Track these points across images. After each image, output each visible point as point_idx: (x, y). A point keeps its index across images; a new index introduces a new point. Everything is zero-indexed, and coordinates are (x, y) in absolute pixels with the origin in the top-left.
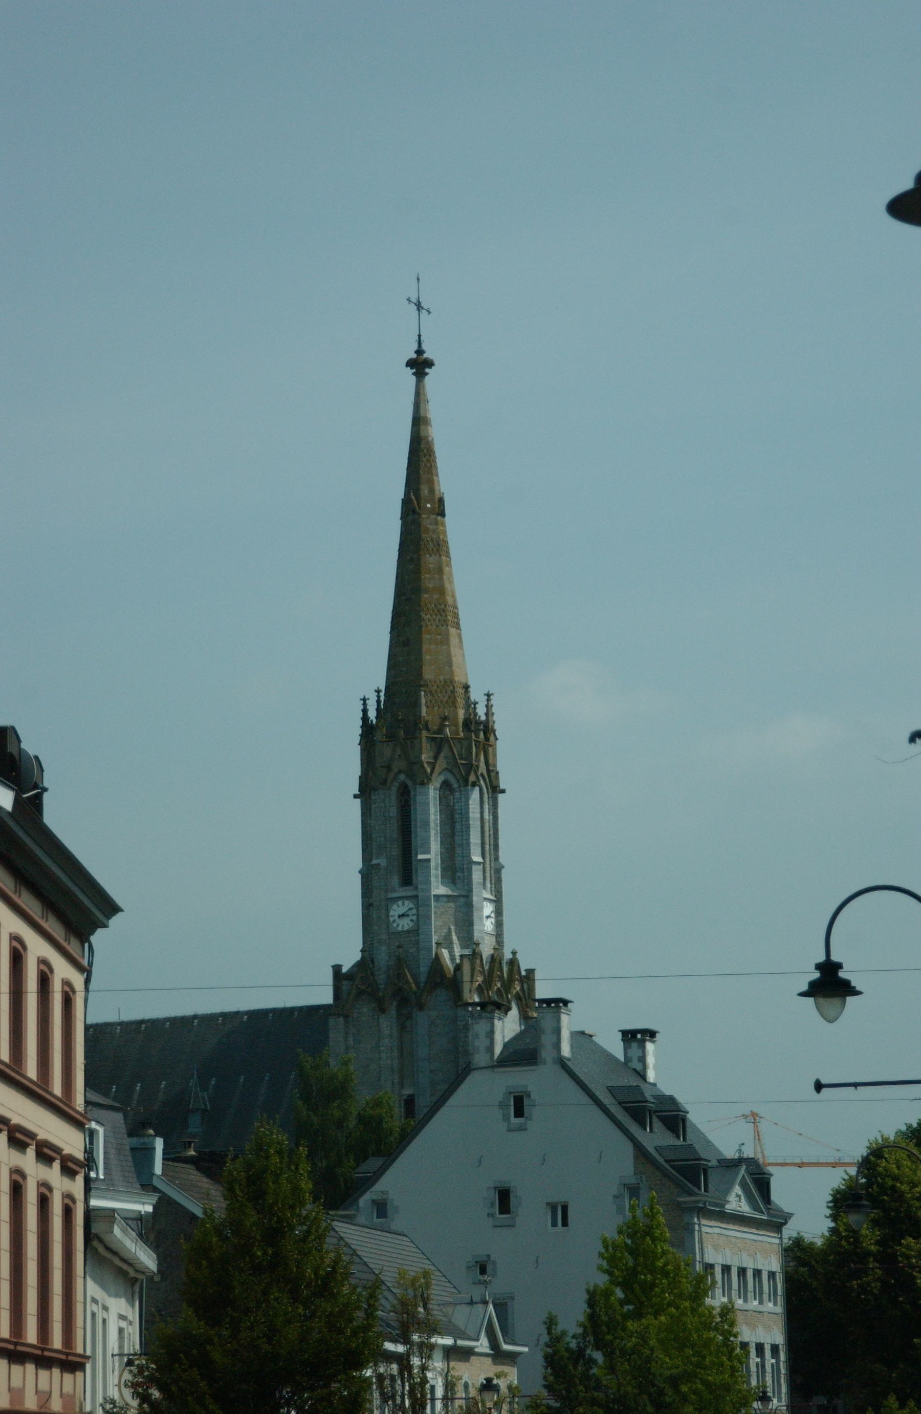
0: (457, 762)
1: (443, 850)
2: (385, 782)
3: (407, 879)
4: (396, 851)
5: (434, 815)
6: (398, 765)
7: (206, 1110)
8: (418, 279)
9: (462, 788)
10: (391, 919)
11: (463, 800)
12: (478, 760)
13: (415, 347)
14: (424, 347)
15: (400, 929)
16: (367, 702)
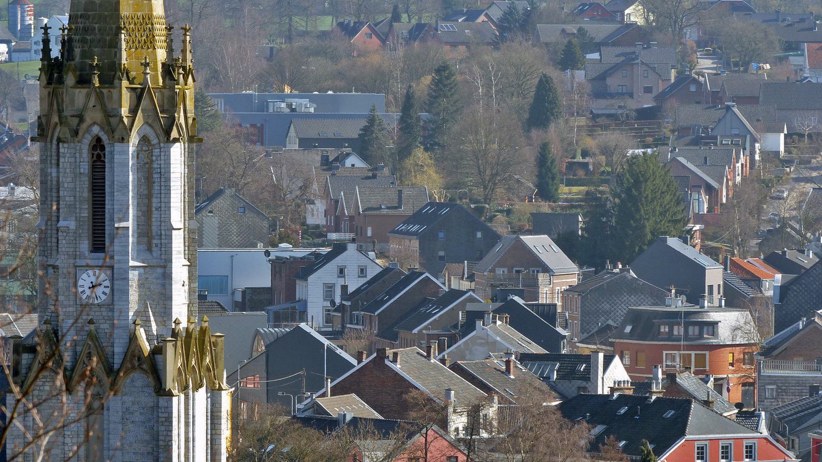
0: (158, 116)
1: (140, 214)
2: (76, 133)
3: (99, 244)
4: (85, 212)
6: (93, 115)
9: (162, 145)
10: (80, 290)
11: (162, 158)
16: (49, 31)
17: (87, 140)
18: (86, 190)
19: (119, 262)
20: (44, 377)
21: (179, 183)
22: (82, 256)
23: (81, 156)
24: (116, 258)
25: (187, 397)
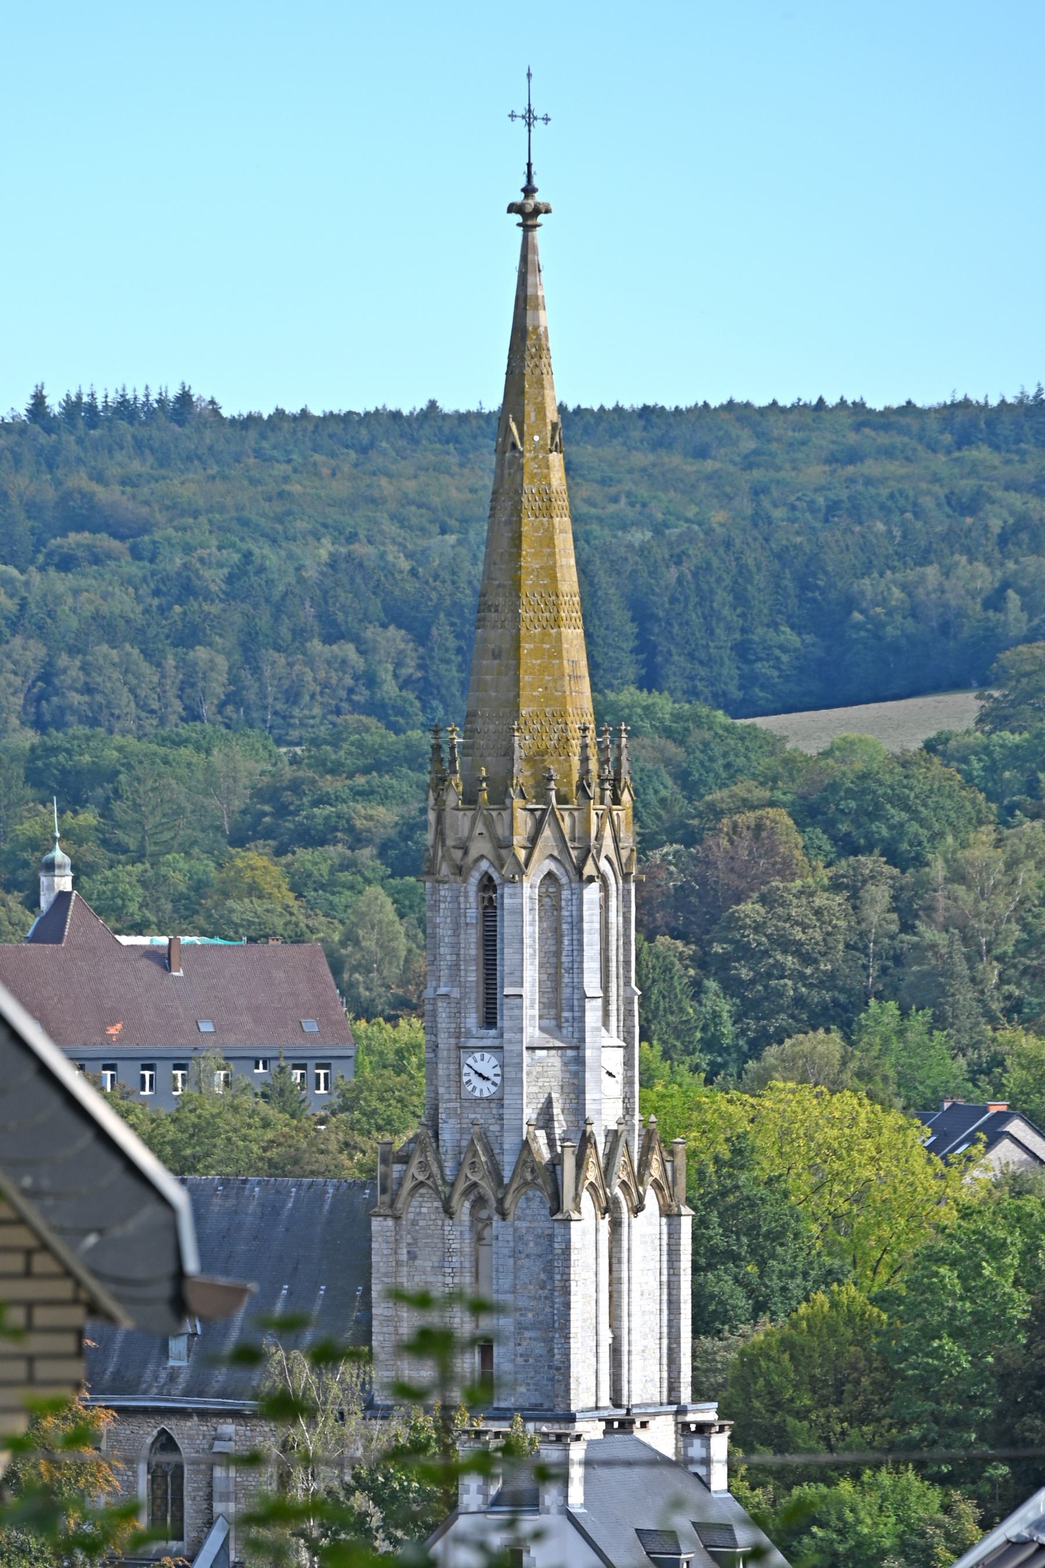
1: (545, 977)
3: (490, 1020)
5: (531, 929)
6: (480, 847)
7: (196, 1334)
8: (529, 75)
12: (599, 837)
13: (523, 182)
14: (536, 182)
15: (477, 1094)
17: (474, 878)
18: (473, 946)
19: (510, 1042)
20: (422, 1195)
21: (506, 930)
22: (469, 1035)
23: (466, 901)
24: (506, 1036)
25: (616, 1225)
